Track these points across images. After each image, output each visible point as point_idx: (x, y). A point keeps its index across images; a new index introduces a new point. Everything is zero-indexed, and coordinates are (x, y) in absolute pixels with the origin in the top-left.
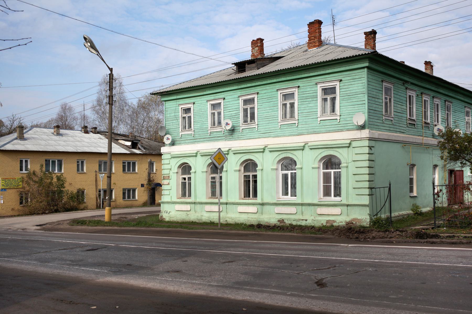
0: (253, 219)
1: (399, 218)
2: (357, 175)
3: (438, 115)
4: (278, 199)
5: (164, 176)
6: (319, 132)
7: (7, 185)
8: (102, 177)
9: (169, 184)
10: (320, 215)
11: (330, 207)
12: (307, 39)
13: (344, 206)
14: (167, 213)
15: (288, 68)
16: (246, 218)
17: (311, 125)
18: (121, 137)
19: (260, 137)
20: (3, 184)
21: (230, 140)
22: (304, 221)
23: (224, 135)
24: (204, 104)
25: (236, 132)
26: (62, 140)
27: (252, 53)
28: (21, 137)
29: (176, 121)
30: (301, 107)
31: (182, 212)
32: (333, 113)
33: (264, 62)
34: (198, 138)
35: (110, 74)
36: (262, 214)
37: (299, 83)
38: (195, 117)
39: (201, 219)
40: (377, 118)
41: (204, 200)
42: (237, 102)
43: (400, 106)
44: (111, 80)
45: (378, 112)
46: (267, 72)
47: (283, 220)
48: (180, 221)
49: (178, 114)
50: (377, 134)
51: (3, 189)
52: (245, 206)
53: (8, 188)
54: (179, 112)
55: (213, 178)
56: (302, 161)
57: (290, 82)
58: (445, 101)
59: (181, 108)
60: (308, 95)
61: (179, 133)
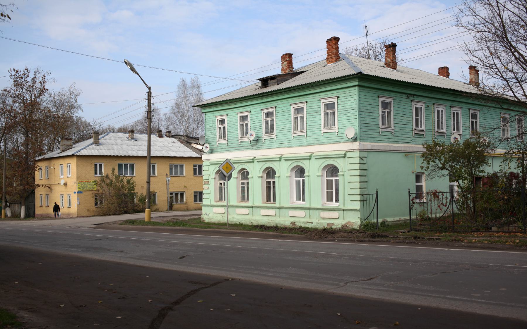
0: (272, 222)
1: (399, 222)
2: (351, 183)
3: (458, 124)
4: (292, 203)
5: (204, 182)
6: (322, 143)
7: (83, 188)
8: (168, 180)
9: (208, 189)
10: (323, 219)
11: (330, 211)
12: (326, 56)
13: (341, 210)
14: (207, 215)
15: (322, 80)
16: (267, 221)
17: (316, 137)
18: (196, 140)
19: (278, 147)
20: (79, 186)
21: (255, 149)
22: (311, 224)
23: (251, 145)
24: (235, 116)
25: (260, 142)
26: (135, 145)
27: (282, 67)
28: (97, 142)
29: (214, 131)
30: (308, 120)
31: (218, 214)
32: (328, 127)
33: (285, 77)
34: (230, 147)
35: (148, 92)
36: (279, 217)
37: (306, 99)
38: (228, 127)
39: (233, 221)
40: (371, 131)
41: (235, 204)
42: (260, 115)
43: (402, 118)
44: (149, 97)
45: (373, 126)
46: (304, 84)
47: (295, 223)
48: (216, 222)
49: (214, 125)
50: (369, 145)
51: (80, 191)
52: (267, 209)
53: (84, 190)
54: (216, 123)
55: (243, 184)
56: (309, 169)
57: (300, 97)
58: (469, 109)
59: (218, 119)
60: (314, 109)
61: (216, 142)
